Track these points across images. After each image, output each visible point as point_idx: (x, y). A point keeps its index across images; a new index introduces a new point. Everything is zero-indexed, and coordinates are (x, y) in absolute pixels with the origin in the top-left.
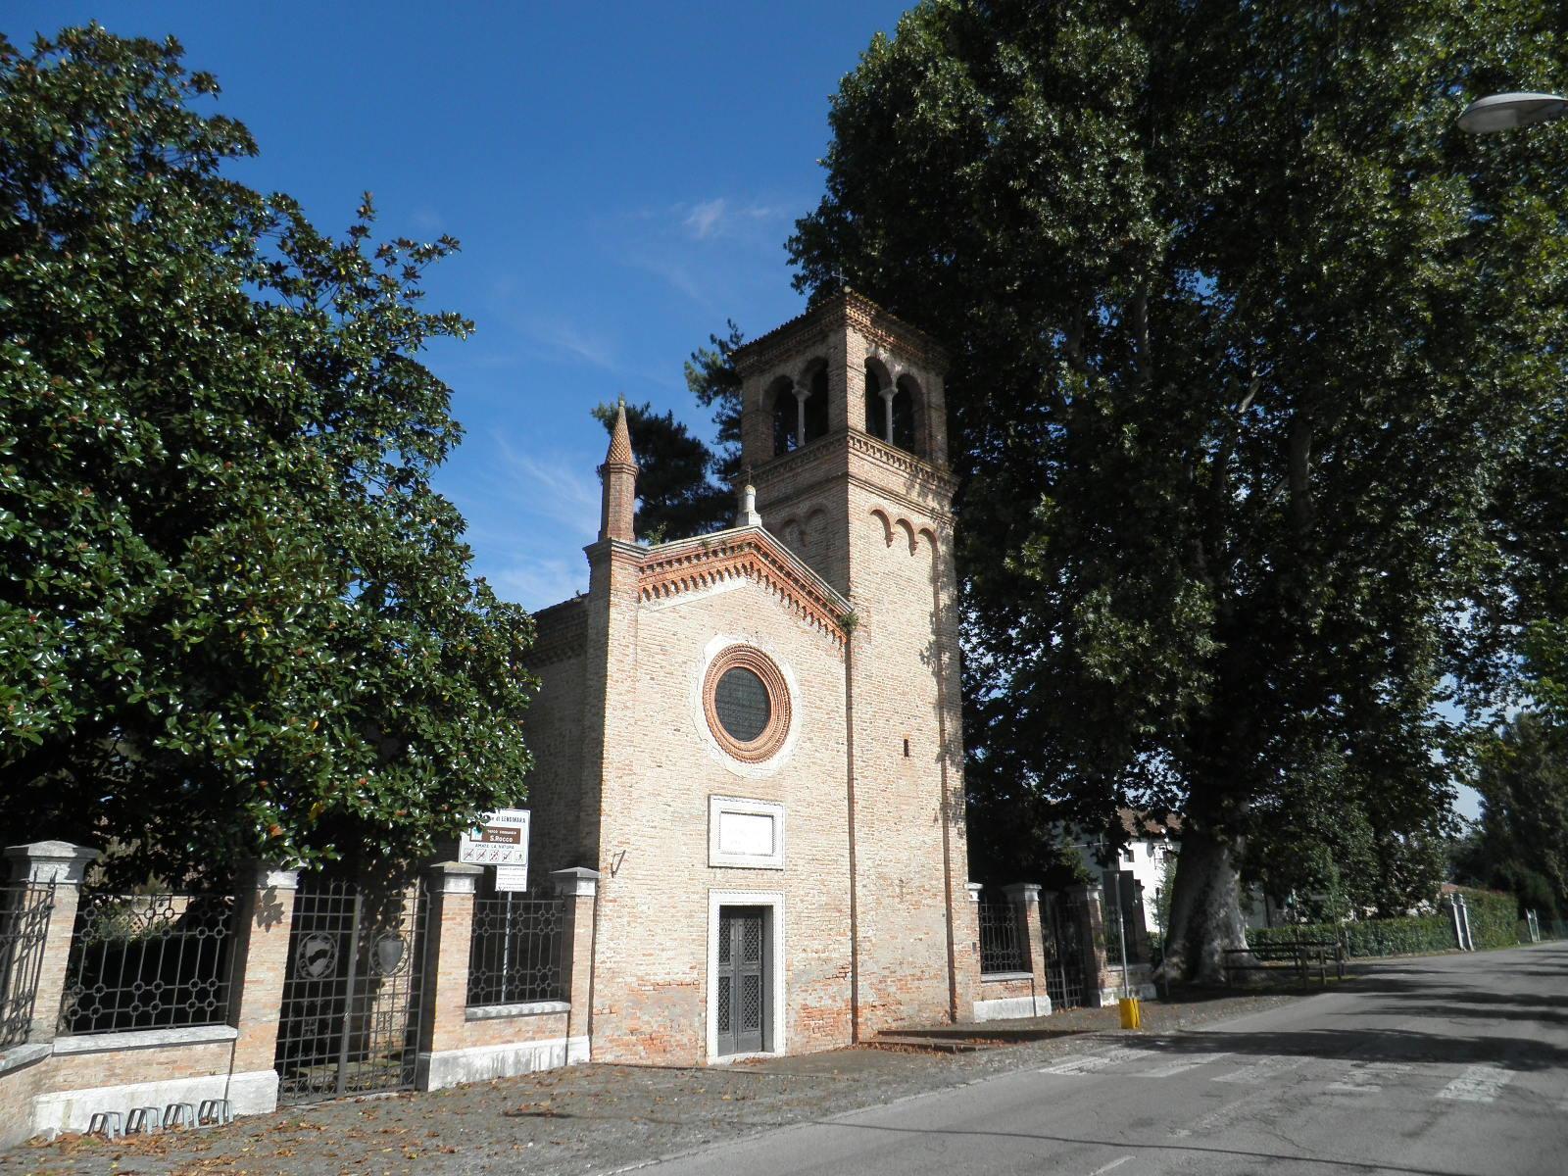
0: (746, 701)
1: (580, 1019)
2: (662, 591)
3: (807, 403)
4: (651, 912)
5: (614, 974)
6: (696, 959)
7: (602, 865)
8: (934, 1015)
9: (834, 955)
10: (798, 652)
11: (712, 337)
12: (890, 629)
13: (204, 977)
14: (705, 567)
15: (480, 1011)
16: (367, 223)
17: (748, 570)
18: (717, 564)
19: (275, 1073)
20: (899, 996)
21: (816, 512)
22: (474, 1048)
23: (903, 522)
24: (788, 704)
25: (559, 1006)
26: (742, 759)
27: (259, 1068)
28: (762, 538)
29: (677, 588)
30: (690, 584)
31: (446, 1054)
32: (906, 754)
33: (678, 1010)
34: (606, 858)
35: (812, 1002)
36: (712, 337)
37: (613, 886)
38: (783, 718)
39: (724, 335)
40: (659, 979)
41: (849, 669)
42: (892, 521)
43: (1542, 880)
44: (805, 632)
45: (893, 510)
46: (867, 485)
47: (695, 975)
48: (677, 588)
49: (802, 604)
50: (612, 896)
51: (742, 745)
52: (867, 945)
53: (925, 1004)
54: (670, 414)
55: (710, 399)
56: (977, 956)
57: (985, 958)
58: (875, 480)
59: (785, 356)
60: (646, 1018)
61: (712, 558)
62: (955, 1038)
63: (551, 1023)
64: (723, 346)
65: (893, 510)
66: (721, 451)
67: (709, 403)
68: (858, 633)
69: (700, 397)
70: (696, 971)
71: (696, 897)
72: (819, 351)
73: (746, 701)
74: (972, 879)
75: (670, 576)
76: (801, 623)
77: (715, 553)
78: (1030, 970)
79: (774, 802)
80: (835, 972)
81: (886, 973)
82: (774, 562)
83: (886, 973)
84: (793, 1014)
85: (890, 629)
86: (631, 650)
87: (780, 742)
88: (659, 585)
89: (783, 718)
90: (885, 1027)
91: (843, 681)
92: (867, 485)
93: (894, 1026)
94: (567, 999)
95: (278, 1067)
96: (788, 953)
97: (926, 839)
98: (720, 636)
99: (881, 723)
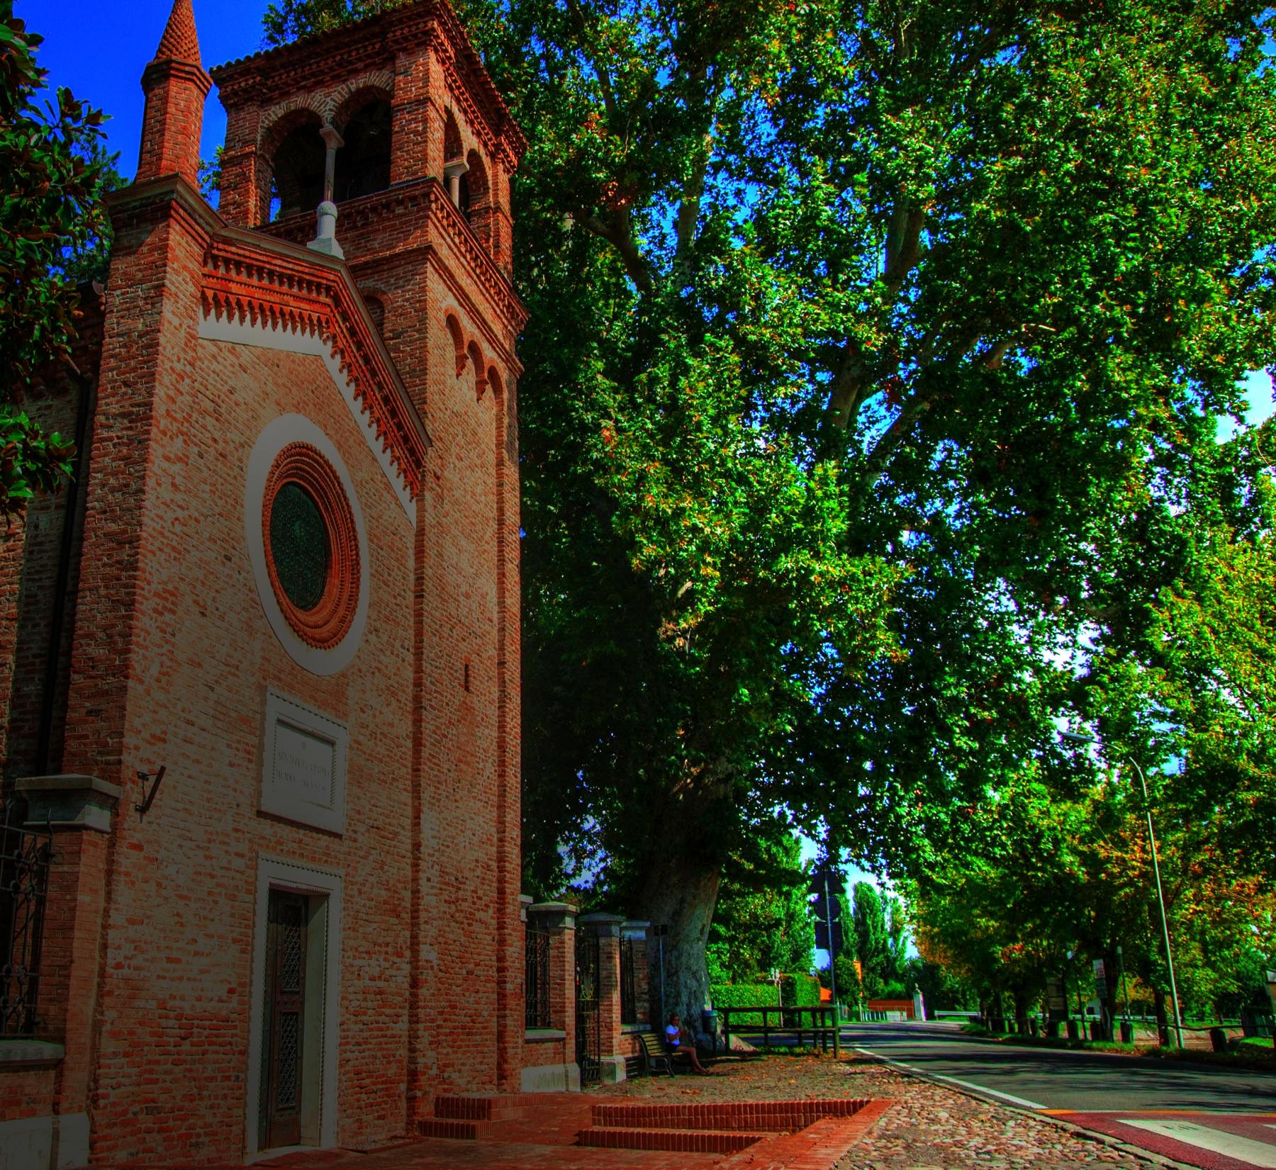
3: (339, 153)
25: (48, 1050)
38: (348, 585)
51: (301, 614)
70: (235, 997)
72: (376, 79)
89: (348, 585)
94: (59, 1037)
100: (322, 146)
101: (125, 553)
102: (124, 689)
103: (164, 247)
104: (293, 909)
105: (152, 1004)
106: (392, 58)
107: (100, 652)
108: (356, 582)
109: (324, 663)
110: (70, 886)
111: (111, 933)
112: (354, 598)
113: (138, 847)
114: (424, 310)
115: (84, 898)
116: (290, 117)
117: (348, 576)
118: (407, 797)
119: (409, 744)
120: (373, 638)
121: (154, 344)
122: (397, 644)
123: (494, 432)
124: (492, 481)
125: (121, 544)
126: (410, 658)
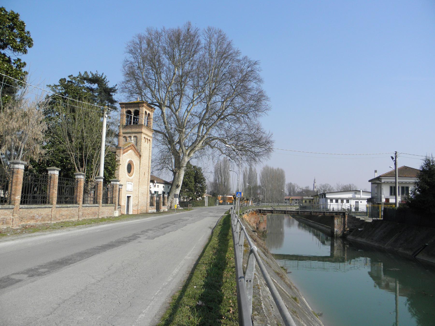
0: (130, 168)
17: (131, 149)
53: (144, 209)
73: (130, 168)
109: (131, 178)
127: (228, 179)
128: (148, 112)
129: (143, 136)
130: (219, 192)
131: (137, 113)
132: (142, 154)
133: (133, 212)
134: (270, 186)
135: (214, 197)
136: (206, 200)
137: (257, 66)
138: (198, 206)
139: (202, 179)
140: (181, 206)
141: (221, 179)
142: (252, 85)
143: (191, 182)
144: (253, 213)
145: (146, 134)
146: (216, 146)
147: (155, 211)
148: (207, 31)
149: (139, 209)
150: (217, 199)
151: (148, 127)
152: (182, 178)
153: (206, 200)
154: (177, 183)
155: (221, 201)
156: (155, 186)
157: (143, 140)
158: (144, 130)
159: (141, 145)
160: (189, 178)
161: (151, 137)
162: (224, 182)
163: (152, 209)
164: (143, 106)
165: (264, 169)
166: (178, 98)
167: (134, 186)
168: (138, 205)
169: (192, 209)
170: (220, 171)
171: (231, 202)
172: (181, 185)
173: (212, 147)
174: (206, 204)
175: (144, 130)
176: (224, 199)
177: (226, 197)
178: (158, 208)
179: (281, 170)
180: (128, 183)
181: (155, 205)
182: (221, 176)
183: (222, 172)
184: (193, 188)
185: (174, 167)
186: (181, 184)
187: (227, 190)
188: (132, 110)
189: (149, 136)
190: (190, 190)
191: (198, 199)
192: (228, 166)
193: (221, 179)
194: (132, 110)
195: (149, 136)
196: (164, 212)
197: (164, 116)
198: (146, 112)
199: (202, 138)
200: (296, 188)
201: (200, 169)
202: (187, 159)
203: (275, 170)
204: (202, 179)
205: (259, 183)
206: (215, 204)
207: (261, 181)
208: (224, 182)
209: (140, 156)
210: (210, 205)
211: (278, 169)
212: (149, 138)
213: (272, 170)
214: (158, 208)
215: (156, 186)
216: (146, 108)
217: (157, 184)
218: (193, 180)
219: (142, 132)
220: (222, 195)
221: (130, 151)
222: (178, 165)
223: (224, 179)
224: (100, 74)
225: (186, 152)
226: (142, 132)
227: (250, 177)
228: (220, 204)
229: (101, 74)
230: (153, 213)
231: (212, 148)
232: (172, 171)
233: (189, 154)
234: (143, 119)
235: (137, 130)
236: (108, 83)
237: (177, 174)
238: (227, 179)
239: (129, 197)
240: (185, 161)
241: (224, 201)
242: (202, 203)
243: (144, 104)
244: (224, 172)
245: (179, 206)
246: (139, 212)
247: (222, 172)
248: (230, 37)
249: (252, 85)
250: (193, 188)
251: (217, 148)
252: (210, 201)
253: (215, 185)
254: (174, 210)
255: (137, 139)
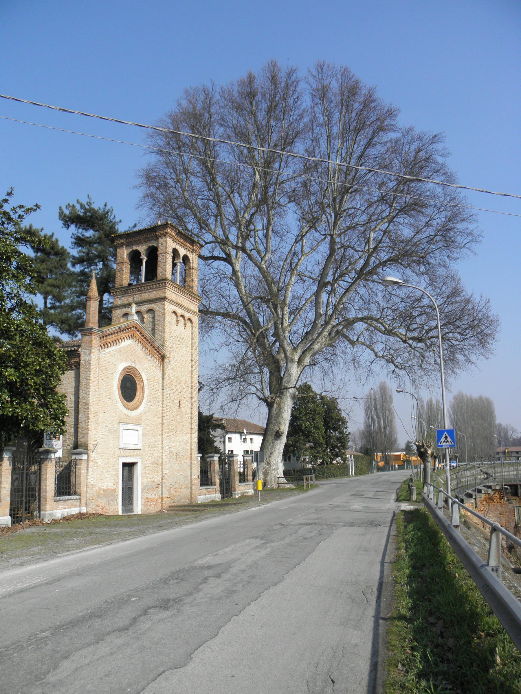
0: (129, 387)
1: (84, 501)
2: (106, 346)
4: (102, 465)
5: (93, 486)
6: (115, 481)
7: (89, 448)
8: (187, 502)
9: (156, 480)
10: (147, 370)
11: (78, 201)
12: (176, 358)
13: (66, 484)
14: (119, 336)
15: (58, 498)
16: (9, 199)
17: (132, 337)
18: (123, 335)
19: (10, 517)
20: (175, 494)
21: (150, 311)
22: (55, 509)
23: (182, 316)
24: (143, 388)
25: (78, 497)
26: (129, 409)
27: (6, 516)
28: (138, 324)
29: (108, 346)
30: (115, 343)
31: (50, 512)
32: (179, 407)
33: (110, 498)
34: (91, 447)
35: (149, 496)
36: (78, 201)
37: (92, 455)
38: (141, 393)
39: (84, 201)
40: (105, 488)
41: (163, 374)
42: (179, 315)
43: (343, 151)
44: (149, 360)
45: (180, 311)
46: (172, 302)
47: (115, 487)
48: (111, 345)
49: (149, 350)
50: (92, 459)
51: (128, 404)
52: (166, 476)
53: (182, 496)
54: (53, 234)
55: (69, 226)
56: (199, 480)
57: (201, 481)
58: (174, 299)
59: (138, 243)
60: (101, 501)
61: (122, 333)
62: (194, 509)
63: (75, 502)
64: (82, 206)
65: (180, 311)
66: (75, 252)
67: (68, 228)
68: (166, 360)
69: (64, 224)
71: (115, 459)
73: (129, 387)
74: (199, 453)
75: (108, 340)
76: (148, 357)
77: (123, 331)
78: (215, 485)
79: (138, 425)
80: (156, 486)
81: (171, 486)
82: (141, 333)
83: (171, 486)
84: (143, 500)
85: (176, 358)
86: (97, 369)
87: (141, 403)
88: (105, 344)
89: (141, 393)
90: (170, 505)
91: (161, 379)
92: (172, 302)
93: (173, 504)
94: (80, 495)
95: (10, 515)
96: (142, 479)
97: (185, 438)
98: (123, 362)
99: (172, 394)
100: (141, 261)
101: (87, 407)
102: (88, 433)
103: (91, 342)
104: (129, 467)
105: (97, 488)
106: (158, 238)
107: (84, 426)
108: (144, 392)
109: (133, 414)
110: (80, 469)
111: (88, 477)
112: (143, 397)
113: (92, 461)
114: (164, 314)
115: (83, 471)
116: (133, 251)
117: (142, 391)
118: (194, 357)
119: (161, 425)
120: (149, 403)
121: (90, 364)
122: (156, 403)
123: (190, 334)
124: (189, 350)
125: (86, 405)
126: (161, 405)
127: (391, 422)
128: (182, 252)
129: (169, 307)
130: (376, 447)
131: (153, 253)
132: (167, 354)
133: (145, 504)
134: (470, 429)
135: (366, 457)
136: (351, 463)
137: (438, 146)
138: (335, 476)
139: (339, 420)
140: (289, 481)
141: (379, 422)
142: (431, 186)
143: (316, 428)
144: (491, 499)
145: (178, 305)
146: (361, 339)
147: (217, 496)
148: (315, 73)
149: (166, 494)
150: (373, 459)
151: (185, 286)
152: (287, 416)
153: (351, 463)
154: (276, 428)
155: (381, 464)
156: (245, 439)
157: (170, 319)
158: (170, 293)
159: (163, 331)
160: (314, 420)
161: (194, 313)
162: (385, 428)
163: (210, 492)
164: (165, 235)
165: (455, 398)
166: (259, 224)
167: (144, 435)
168: (160, 485)
169: (317, 486)
170: (376, 408)
171: (401, 463)
172: (286, 433)
173: (353, 343)
174: (352, 471)
175: (170, 293)
176: (386, 459)
177: (390, 456)
178: (226, 488)
179: (486, 399)
180: (122, 426)
181: (218, 481)
182: (379, 418)
183: (379, 407)
184: (322, 441)
185: (267, 393)
186: (285, 428)
187: (390, 443)
188: (142, 249)
189: (188, 311)
190: (317, 444)
191: (335, 462)
192: (388, 397)
193: (379, 422)
194: (142, 249)
195: (188, 311)
196: (245, 499)
197: (237, 278)
198: (175, 251)
199: (327, 323)
200: (510, 433)
201: (334, 400)
202: (294, 370)
203: (476, 400)
204: (339, 420)
205: (448, 425)
206: (369, 468)
207: (452, 421)
208: (385, 428)
209: (163, 358)
210: (359, 472)
211: (481, 398)
212: (187, 315)
213: (470, 400)
214: (226, 488)
215: (248, 440)
216: (175, 240)
217: (249, 437)
218: (321, 424)
219: (164, 299)
220: (382, 452)
221: (128, 343)
222: (277, 386)
223: (384, 422)
224: (97, 206)
225: (293, 354)
226: (164, 299)
227: (429, 416)
228: (379, 469)
229: (102, 207)
230: (213, 505)
231: (353, 346)
232: (265, 400)
233: (300, 361)
234: (166, 268)
235: (153, 295)
236: (120, 224)
237: (275, 406)
238: (389, 423)
239: (129, 467)
240: (290, 375)
241: (387, 463)
242: (343, 470)
243: (168, 230)
244: (383, 409)
245: (284, 480)
246: (167, 503)
247: (379, 407)
248: (367, 79)
249: (431, 186)
250: (322, 441)
251: (363, 344)
252: (359, 465)
253: (368, 434)
254: (272, 490)
255: (154, 317)
